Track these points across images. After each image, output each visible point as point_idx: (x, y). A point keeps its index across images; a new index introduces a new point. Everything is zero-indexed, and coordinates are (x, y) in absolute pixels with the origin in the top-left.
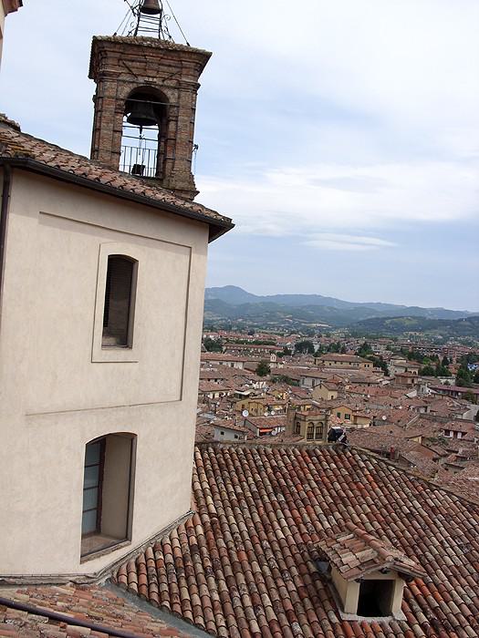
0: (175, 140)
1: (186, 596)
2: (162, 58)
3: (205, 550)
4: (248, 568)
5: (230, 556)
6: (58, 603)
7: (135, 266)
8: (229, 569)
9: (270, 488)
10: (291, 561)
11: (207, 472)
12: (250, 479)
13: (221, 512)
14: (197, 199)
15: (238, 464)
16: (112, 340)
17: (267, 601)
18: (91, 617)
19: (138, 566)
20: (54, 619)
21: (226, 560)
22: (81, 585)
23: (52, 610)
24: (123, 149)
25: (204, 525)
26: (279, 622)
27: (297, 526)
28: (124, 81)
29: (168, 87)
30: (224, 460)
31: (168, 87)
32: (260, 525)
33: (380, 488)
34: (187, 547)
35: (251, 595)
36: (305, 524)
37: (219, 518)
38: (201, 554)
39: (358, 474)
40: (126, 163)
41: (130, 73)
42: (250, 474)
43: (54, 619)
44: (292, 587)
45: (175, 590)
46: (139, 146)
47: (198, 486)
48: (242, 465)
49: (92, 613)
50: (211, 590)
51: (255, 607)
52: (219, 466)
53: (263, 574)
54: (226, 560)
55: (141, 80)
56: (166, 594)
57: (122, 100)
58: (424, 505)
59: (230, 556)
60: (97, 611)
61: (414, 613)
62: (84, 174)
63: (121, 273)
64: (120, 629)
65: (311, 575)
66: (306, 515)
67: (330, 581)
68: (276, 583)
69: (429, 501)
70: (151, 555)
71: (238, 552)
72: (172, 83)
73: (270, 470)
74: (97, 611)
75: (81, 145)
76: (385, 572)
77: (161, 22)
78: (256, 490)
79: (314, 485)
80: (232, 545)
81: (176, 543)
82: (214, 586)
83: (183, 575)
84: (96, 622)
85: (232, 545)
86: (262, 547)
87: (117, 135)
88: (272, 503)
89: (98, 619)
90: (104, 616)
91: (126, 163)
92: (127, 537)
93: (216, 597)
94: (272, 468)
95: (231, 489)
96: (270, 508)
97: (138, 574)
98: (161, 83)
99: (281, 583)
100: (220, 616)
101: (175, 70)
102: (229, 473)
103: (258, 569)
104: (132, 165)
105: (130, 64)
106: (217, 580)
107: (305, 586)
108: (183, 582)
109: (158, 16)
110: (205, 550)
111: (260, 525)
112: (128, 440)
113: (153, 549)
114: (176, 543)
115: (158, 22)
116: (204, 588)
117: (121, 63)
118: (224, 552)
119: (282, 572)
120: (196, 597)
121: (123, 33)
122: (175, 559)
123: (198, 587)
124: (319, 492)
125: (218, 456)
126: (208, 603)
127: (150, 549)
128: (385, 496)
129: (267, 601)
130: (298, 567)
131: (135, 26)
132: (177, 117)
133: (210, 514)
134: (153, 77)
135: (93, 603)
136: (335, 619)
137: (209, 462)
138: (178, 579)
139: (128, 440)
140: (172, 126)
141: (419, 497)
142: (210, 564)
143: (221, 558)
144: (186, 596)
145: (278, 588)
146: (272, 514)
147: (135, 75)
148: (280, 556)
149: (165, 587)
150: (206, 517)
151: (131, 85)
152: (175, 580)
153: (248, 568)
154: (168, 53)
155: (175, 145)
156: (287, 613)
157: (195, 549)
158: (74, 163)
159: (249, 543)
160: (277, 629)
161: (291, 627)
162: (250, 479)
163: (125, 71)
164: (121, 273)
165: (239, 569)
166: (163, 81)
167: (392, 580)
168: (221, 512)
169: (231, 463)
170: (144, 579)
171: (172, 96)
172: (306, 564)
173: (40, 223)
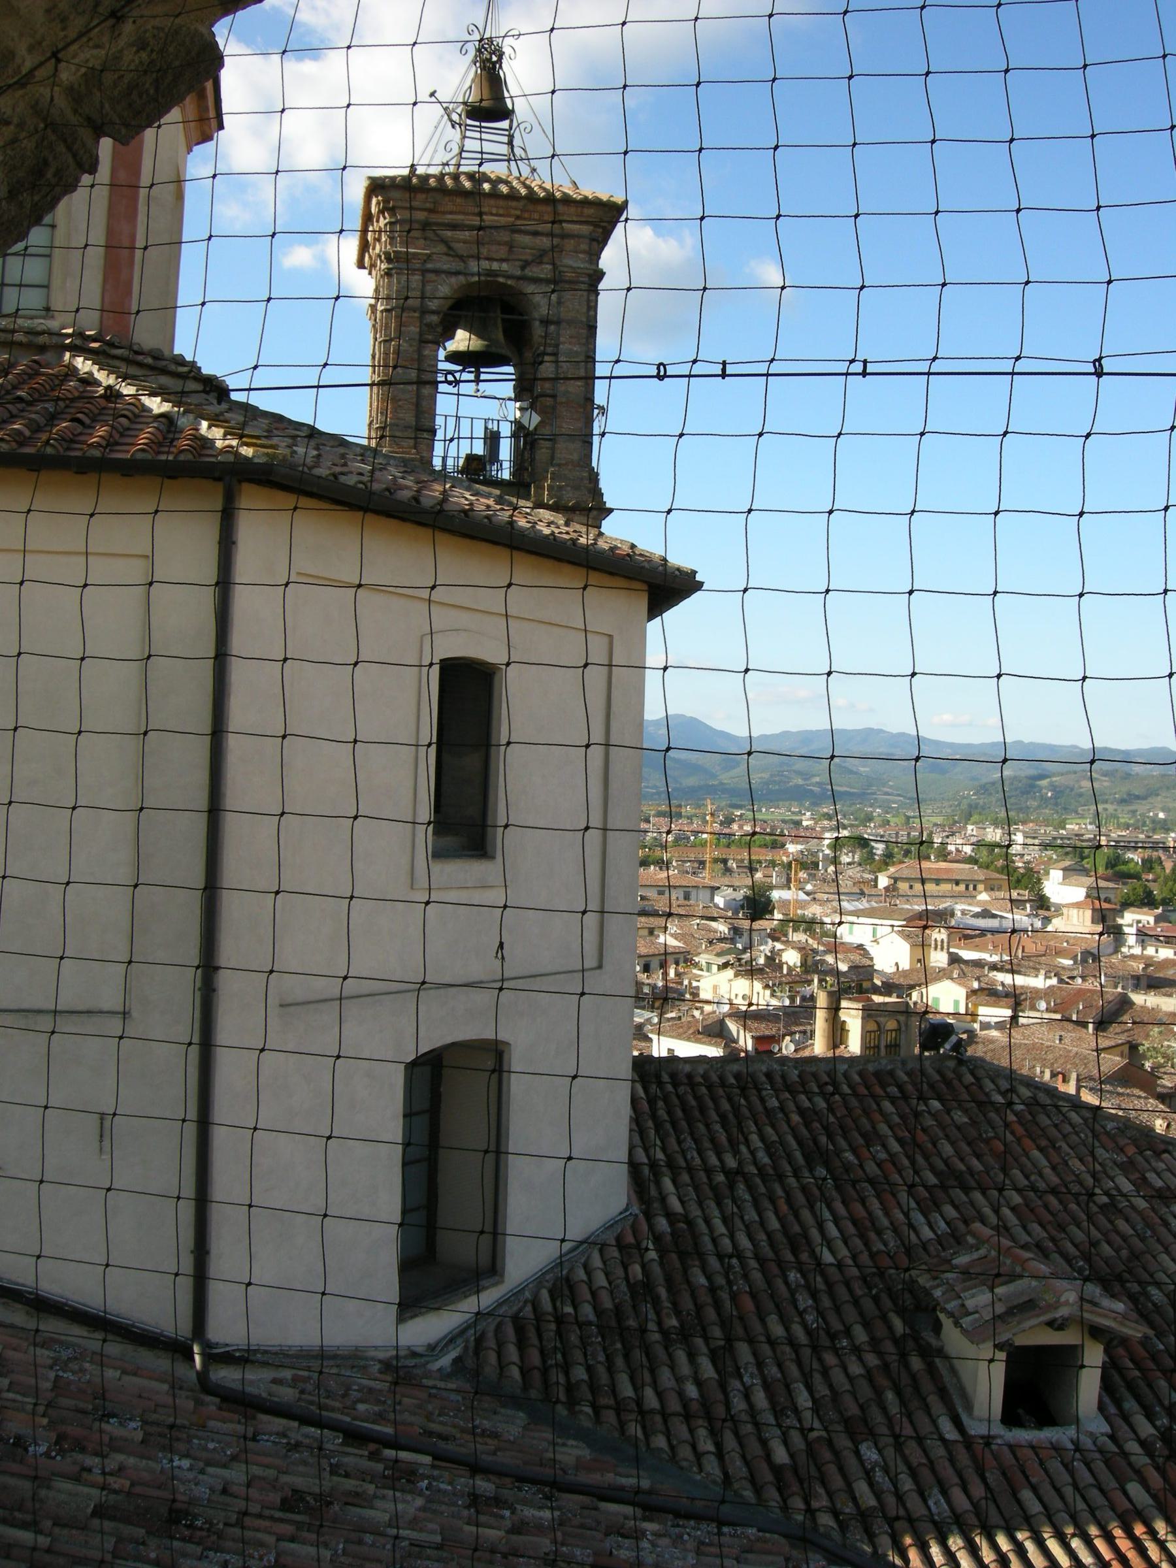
0: (554, 396)
1: (627, 1391)
2: (518, 218)
3: (663, 1292)
4: (757, 1327)
5: (717, 1305)
6: (361, 1407)
7: (496, 678)
8: (717, 1332)
9: (798, 1155)
10: (850, 1313)
11: (658, 1126)
12: (754, 1138)
13: (695, 1212)
14: (610, 527)
15: (726, 1106)
16: (449, 841)
17: (803, 1400)
18: (430, 1434)
19: (520, 1330)
20: (354, 1437)
21: (711, 1314)
22: (401, 1370)
23: (348, 1419)
24: (439, 421)
25: (657, 1238)
26: (830, 1443)
27: (862, 1236)
28: (437, 272)
29: (536, 280)
30: (696, 1097)
31: (536, 280)
32: (779, 1237)
33: (1041, 1150)
34: (624, 1287)
35: (766, 1386)
36: (879, 1233)
37: (690, 1223)
38: (656, 1302)
39: (990, 1122)
40: (452, 448)
41: (451, 252)
42: (754, 1128)
43: (354, 1437)
44: (856, 1369)
45: (604, 1378)
46: (476, 411)
47: (641, 1156)
48: (736, 1109)
49: (434, 1427)
50: (687, 1374)
51: (778, 1413)
52: (684, 1110)
53: (792, 1342)
54: (711, 1314)
55: (473, 266)
56: (585, 1388)
57: (433, 312)
58: (1141, 1183)
59: (717, 1305)
60: (441, 1423)
61: (1126, 1418)
62: (388, 489)
63: (467, 696)
64: (490, 1458)
65: (896, 1341)
66: (880, 1213)
67: (941, 1352)
68: (821, 1360)
69: (1151, 1176)
70: (546, 1303)
71: (734, 1297)
72: (545, 271)
73: (796, 1118)
74: (441, 1423)
75: (349, 416)
76: (1061, 1328)
77: (511, 138)
78: (766, 1160)
79: (895, 1147)
80: (720, 1280)
81: (601, 1280)
82: (685, 1370)
83: (619, 1346)
84: (442, 1444)
85: (720, 1280)
86: (787, 1283)
87: (426, 390)
88: (804, 1189)
89: (441, 1437)
90: (454, 1431)
91: (452, 448)
92: (493, 1269)
93: (692, 1391)
94: (801, 1112)
95: (713, 1160)
96: (800, 1199)
97: (521, 1344)
98: (519, 273)
99: (830, 1359)
100: (702, 1433)
101: (545, 242)
102: (707, 1126)
103: (778, 1330)
104: (463, 455)
105: (449, 233)
106: (692, 1356)
107: (886, 1366)
108: (620, 1362)
109: (505, 124)
110: (663, 1292)
111: (779, 1237)
112: (492, 1057)
113: (551, 1292)
114: (601, 1280)
115: (505, 139)
116: (665, 1376)
117: (430, 234)
118: (705, 1298)
119: (833, 1337)
120: (649, 1392)
121: (430, 166)
122: (599, 1312)
123: (652, 1371)
124: (906, 1162)
125: (682, 1090)
126: (674, 1405)
127: (545, 1294)
128: (1054, 1168)
129: (803, 1400)
130: (866, 1325)
131: (456, 150)
132: (557, 346)
133: (669, 1215)
134: (502, 260)
135: (430, 1407)
136: (950, 1433)
137: (661, 1104)
138: (607, 1357)
139: (492, 1057)
140: (547, 369)
141: (1128, 1167)
142: (674, 1322)
143: (699, 1308)
144: (627, 1391)
145: (825, 1372)
146: (806, 1214)
147: (461, 258)
148: (826, 1302)
149: (580, 1373)
150: (662, 1224)
151: (453, 280)
152: (601, 1358)
153: (757, 1327)
154: (531, 207)
155: (554, 408)
156: (847, 1422)
157: (643, 1290)
158: (576, 518)
159: (757, 1276)
160: (827, 1455)
161: (857, 1453)
162: (754, 1138)
163: (441, 248)
164: (467, 696)
165: (740, 1331)
166: (523, 268)
167: (1075, 1346)
168: (695, 1212)
169: (710, 1104)
170: (535, 1358)
171: (541, 302)
172: (884, 1318)
173: (694, 573)
